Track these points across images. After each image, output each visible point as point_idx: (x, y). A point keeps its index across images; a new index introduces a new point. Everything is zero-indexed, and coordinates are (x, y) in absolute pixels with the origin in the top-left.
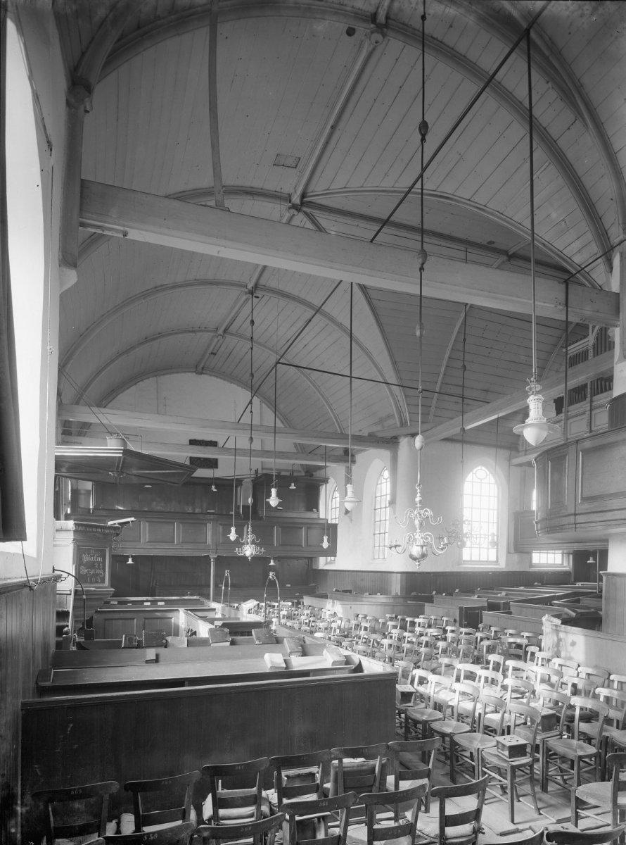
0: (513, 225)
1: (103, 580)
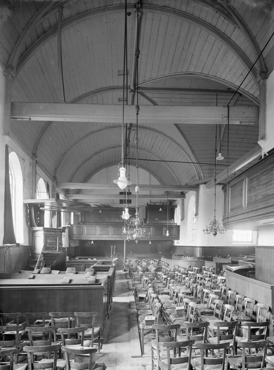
0: (221, 81)
1: (56, 249)
